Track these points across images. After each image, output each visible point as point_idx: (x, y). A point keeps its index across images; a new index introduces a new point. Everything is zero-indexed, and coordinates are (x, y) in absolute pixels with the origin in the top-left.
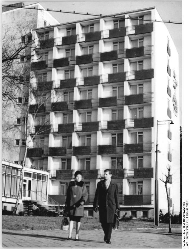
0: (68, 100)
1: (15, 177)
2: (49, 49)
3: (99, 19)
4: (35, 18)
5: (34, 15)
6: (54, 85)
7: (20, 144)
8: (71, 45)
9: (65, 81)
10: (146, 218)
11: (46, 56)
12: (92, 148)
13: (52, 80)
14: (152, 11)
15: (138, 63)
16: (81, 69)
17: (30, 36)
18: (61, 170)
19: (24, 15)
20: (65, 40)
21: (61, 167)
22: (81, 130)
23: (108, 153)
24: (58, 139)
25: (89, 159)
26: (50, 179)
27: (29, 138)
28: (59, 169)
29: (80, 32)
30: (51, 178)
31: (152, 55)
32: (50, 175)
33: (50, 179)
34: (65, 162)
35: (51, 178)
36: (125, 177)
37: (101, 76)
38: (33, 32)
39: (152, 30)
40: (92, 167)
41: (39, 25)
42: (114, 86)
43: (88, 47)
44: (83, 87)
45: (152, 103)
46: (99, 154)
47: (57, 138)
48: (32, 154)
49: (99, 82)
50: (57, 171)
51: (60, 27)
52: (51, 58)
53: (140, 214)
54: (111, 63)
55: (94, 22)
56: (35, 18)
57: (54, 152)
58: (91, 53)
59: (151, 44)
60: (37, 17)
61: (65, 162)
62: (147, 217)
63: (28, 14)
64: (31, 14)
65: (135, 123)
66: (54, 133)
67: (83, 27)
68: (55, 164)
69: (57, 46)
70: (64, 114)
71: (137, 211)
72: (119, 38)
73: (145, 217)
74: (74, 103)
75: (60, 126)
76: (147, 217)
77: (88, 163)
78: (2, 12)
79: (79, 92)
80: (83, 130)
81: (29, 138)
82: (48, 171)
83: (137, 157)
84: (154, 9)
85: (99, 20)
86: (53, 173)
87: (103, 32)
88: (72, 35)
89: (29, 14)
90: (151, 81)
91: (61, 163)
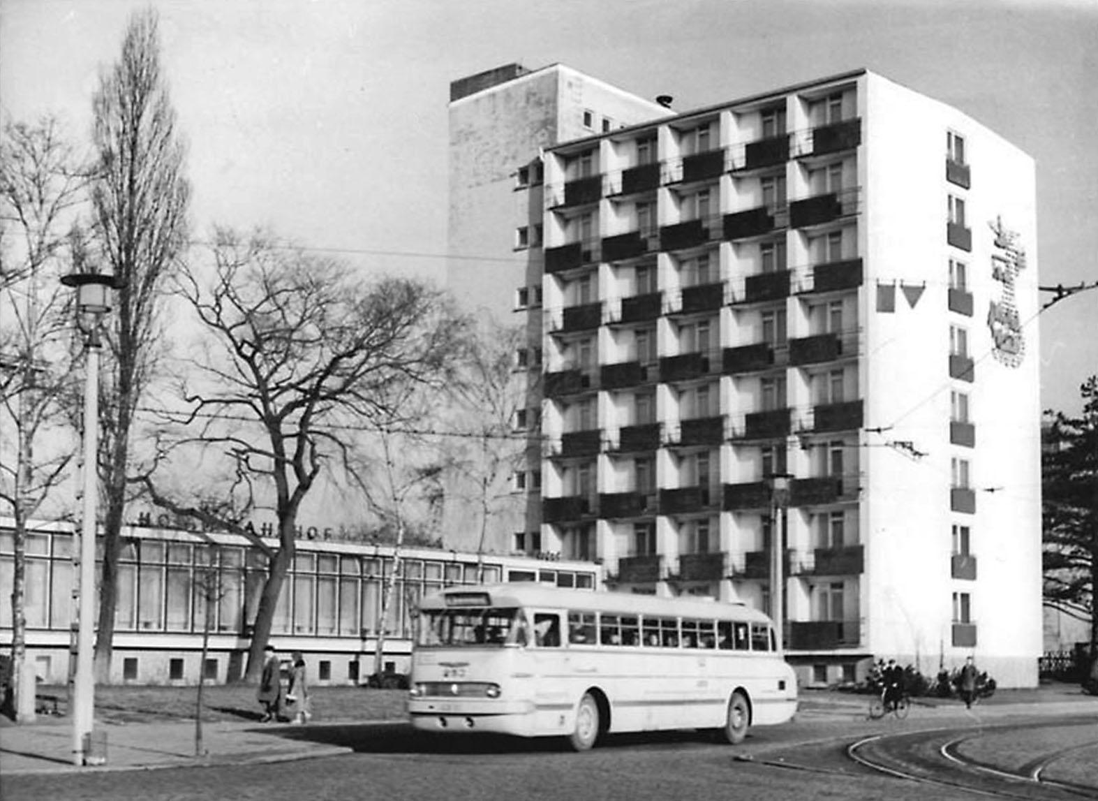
0: (775, 337)
1: (418, 586)
2: (709, 181)
3: (717, 112)
4: (550, 110)
5: (548, 101)
6: (728, 293)
7: (526, 485)
8: (647, 193)
9: (632, 302)
10: (850, 684)
11: (704, 204)
12: (712, 492)
13: (601, 298)
14: (860, 80)
15: (828, 240)
16: (809, 240)
17: (539, 167)
18: (633, 555)
19: (522, 104)
20: (629, 177)
21: (634, 547)
22: (812, 428)
23: (751, 504)
24: (623, 469)
25: (841, 514)
26: (604, 582)
27: (549, 470)
28: (629, 552)
29: (671, 152)
30: (606, 578)
31: (858, 216)
32: (603, 571)
33: (604, 582)
34: (644, 534)
35: (606, 578)
36: (793, 572)
37: (795, 271)
38: (546, 155)
39: (857, 141)
40: (848, 540)
41: (564, 131)
42: (766, 310)
43: (824, 169)
44: (681, 317)
45: (860, 358)
46: (727, 509)
47: (621, 464)
48: (555, 512)
49: (600, 321)
50: (621, 561)
51: (739, 109)
52: (715, 212)
53: (835, 673)
54: (755, 242)
55: (705, 122)
56: (550, 110)
57: (614, 508)
58: (836, 189)
59: (856, 182)
60: (555, 108)
61: (644, 534)
62: (854, 679)
63: (532, 99)
64: (540, 99)
65: (816, 420)
66: (670, 446)
67: (809, 103)
68: (618, 541)
69: (735, 171)
70: (764, 381)
71: (830, 663)
72: (774, 168)
73: (849, 681)
74: (658, 362)
75: (623, 431)
76: (825, 680)
77: (838, 526)
78: (452, 100)
79: (804, 310)
80: (684, 442)
81: (549, 470)
82: (599, 562)
83: (829, 516)
84: (865, 76)
85: (785, 100)
86: (612, 566)
87: (731, 152)
88: (778, 135)
89: (536, 98)
90: (856, 293)
91: (635, 538)
